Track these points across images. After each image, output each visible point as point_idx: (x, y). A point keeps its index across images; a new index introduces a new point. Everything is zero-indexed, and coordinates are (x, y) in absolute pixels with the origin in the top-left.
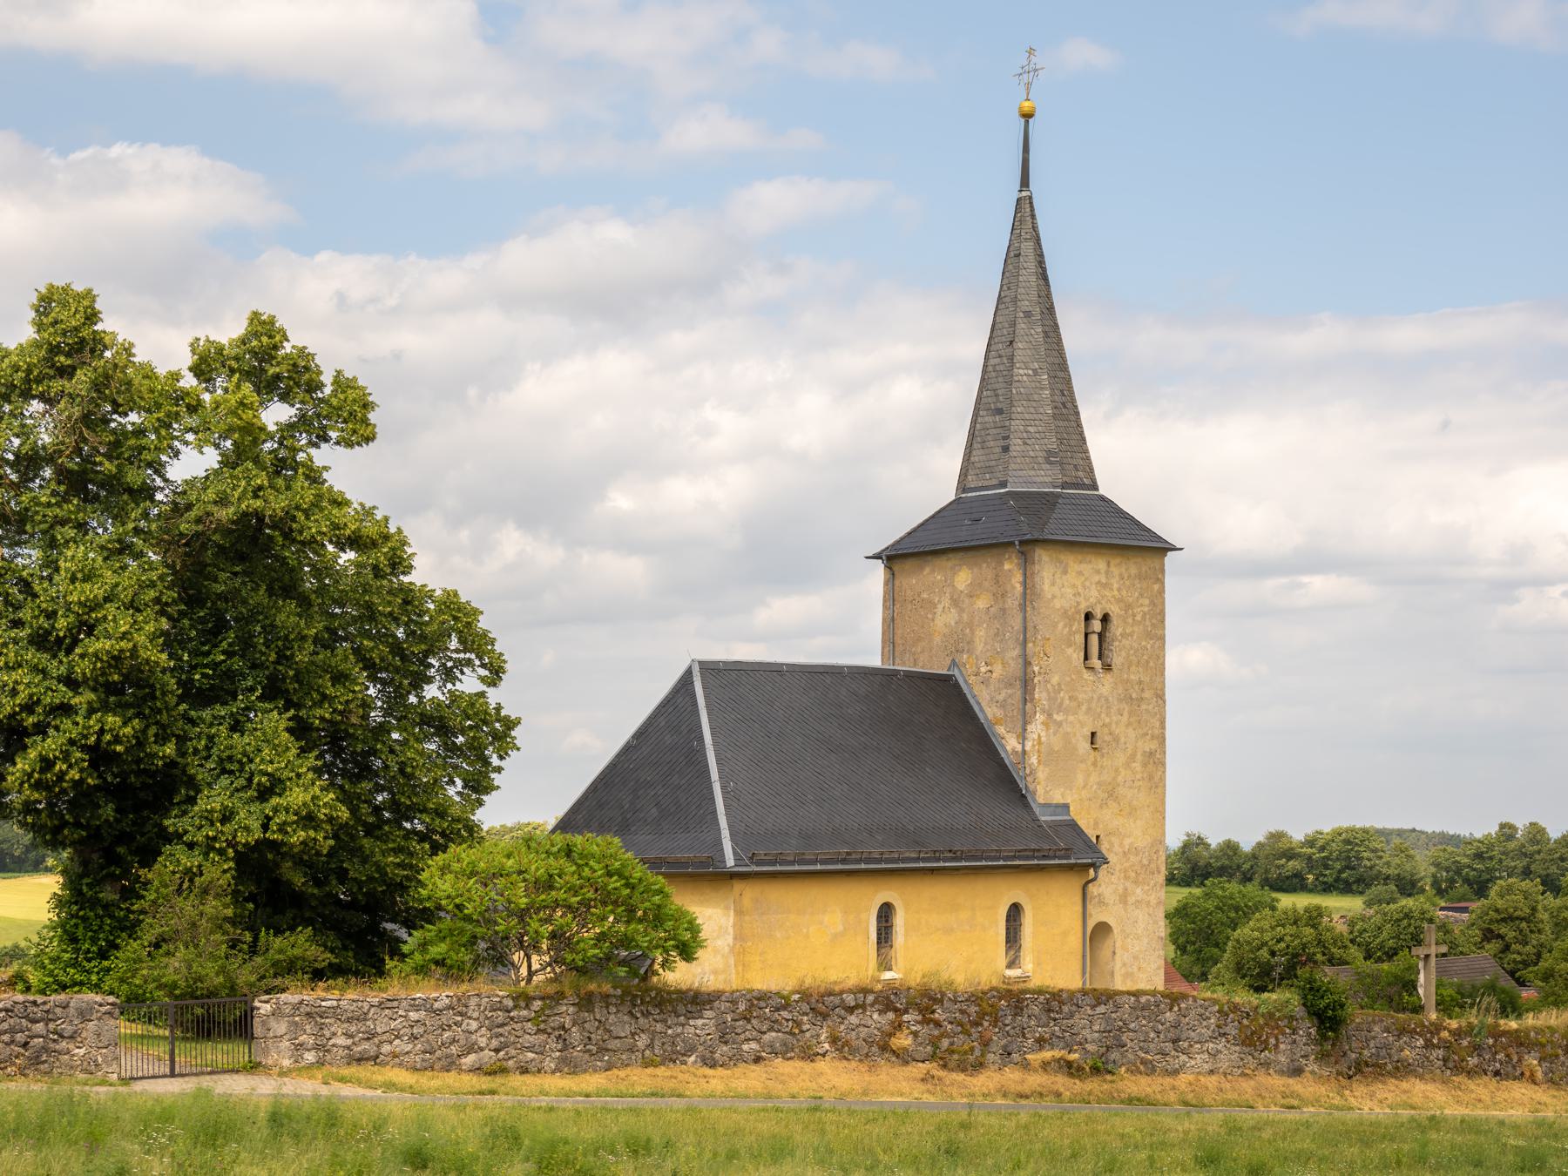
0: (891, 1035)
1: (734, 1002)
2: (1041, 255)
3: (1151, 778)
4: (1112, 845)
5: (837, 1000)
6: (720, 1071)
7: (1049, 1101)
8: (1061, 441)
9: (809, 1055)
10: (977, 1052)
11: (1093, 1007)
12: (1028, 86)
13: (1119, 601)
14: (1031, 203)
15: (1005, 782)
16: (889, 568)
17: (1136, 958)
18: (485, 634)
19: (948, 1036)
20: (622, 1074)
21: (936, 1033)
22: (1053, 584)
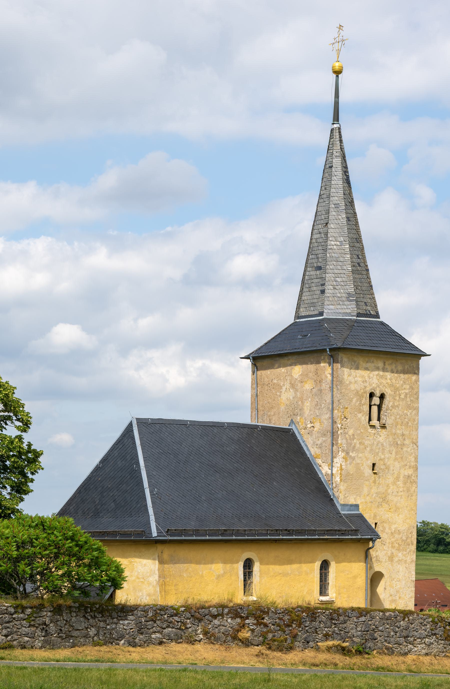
0: (238, 631)
1: (146, 611)
2: (346, 167)
3: (408, 490)
4: (384, 528)
5: (207, 611)
6: (138, 649)
7: (330, 668)
8: (356, 287)
9: (191, 641)
10: (289, 641)
11: (358, 618)
12: (339, 51)
13: (391, 386)
14: (340, 132)
15: (320, 491)
16: (254, 365)
17: (398, 592)
18: (18, 401)
19: (271, 632)
20: (80, 649)
21: (265, 630)
22: (350, 375)
